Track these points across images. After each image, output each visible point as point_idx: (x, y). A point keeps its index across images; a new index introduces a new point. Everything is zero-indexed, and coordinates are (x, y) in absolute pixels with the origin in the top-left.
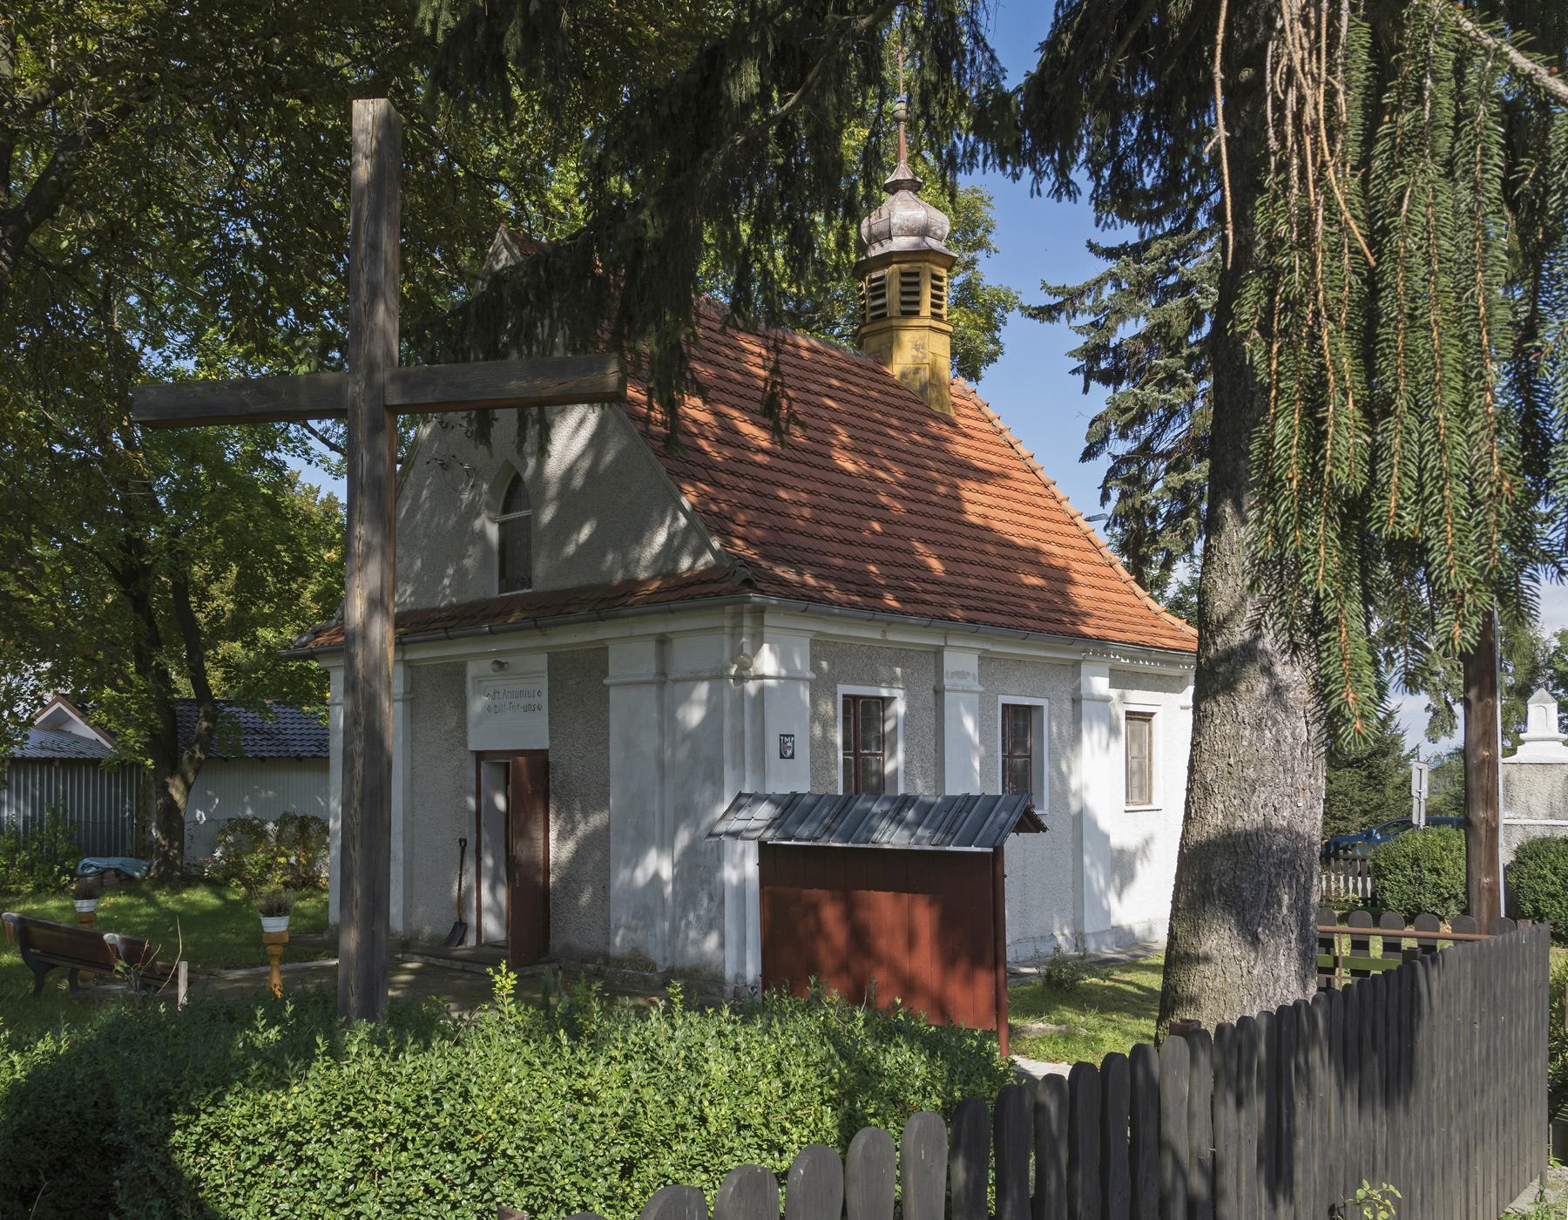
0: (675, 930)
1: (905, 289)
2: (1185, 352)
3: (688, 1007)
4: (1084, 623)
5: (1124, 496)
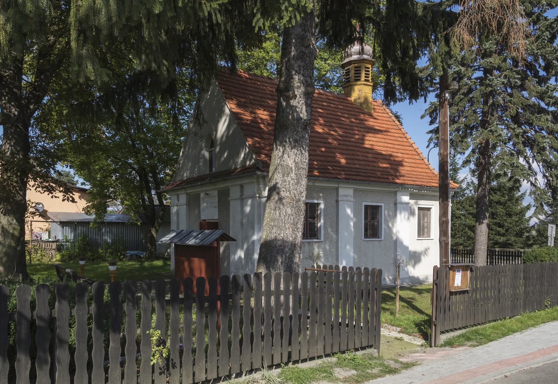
1: (356, 72)
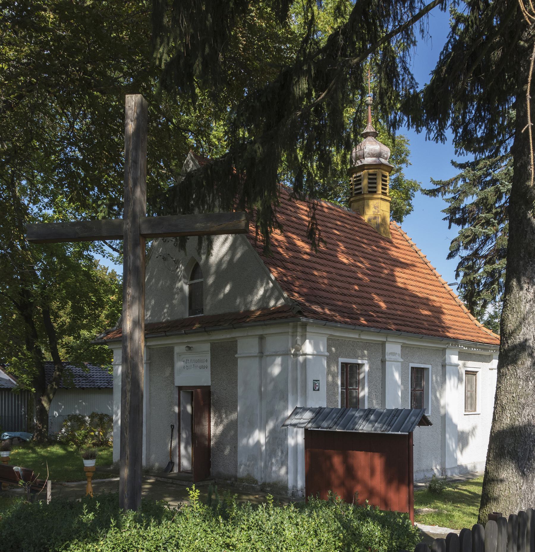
0: (266, 466)
1: (370, 181)
2: (494, 211)
3: (275, 506)
4: (448, 332)
5: (466, 275)
